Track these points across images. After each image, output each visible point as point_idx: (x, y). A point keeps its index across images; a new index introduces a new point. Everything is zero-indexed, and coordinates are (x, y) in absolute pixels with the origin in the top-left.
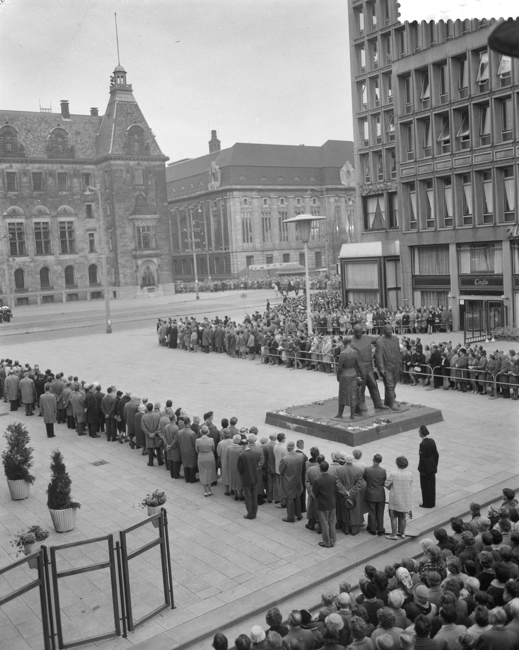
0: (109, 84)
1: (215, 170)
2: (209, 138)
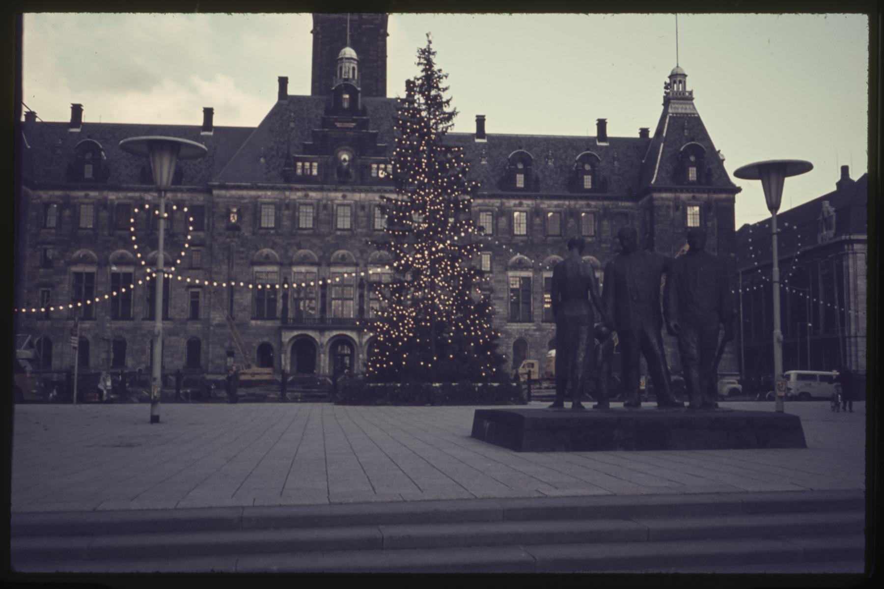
0: (661, 93)
1: (828, 213)
2: (838, 178)
